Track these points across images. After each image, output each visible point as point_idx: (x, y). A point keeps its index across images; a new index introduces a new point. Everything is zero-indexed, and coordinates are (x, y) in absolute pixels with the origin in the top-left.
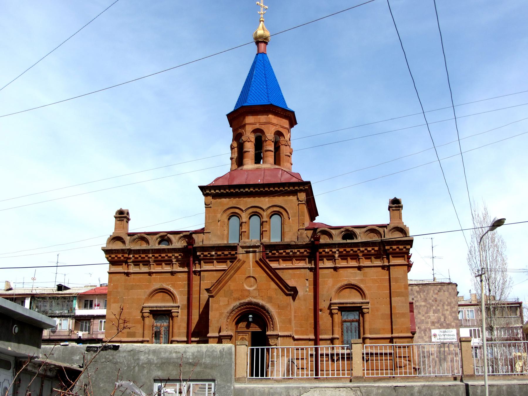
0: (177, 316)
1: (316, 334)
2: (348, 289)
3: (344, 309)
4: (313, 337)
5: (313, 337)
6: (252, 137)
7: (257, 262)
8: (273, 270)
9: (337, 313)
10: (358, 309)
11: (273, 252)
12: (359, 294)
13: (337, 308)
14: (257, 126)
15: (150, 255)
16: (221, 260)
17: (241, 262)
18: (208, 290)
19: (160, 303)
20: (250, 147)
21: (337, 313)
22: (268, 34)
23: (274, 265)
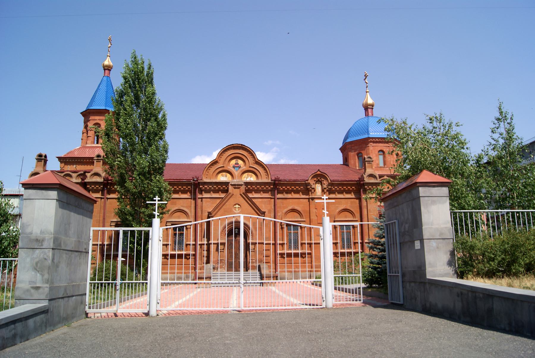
7: (241, 195)
8: (250, 199)
14: (96, 122)
16: (216, 191)
22: (111, 64)
23: (250, 195)
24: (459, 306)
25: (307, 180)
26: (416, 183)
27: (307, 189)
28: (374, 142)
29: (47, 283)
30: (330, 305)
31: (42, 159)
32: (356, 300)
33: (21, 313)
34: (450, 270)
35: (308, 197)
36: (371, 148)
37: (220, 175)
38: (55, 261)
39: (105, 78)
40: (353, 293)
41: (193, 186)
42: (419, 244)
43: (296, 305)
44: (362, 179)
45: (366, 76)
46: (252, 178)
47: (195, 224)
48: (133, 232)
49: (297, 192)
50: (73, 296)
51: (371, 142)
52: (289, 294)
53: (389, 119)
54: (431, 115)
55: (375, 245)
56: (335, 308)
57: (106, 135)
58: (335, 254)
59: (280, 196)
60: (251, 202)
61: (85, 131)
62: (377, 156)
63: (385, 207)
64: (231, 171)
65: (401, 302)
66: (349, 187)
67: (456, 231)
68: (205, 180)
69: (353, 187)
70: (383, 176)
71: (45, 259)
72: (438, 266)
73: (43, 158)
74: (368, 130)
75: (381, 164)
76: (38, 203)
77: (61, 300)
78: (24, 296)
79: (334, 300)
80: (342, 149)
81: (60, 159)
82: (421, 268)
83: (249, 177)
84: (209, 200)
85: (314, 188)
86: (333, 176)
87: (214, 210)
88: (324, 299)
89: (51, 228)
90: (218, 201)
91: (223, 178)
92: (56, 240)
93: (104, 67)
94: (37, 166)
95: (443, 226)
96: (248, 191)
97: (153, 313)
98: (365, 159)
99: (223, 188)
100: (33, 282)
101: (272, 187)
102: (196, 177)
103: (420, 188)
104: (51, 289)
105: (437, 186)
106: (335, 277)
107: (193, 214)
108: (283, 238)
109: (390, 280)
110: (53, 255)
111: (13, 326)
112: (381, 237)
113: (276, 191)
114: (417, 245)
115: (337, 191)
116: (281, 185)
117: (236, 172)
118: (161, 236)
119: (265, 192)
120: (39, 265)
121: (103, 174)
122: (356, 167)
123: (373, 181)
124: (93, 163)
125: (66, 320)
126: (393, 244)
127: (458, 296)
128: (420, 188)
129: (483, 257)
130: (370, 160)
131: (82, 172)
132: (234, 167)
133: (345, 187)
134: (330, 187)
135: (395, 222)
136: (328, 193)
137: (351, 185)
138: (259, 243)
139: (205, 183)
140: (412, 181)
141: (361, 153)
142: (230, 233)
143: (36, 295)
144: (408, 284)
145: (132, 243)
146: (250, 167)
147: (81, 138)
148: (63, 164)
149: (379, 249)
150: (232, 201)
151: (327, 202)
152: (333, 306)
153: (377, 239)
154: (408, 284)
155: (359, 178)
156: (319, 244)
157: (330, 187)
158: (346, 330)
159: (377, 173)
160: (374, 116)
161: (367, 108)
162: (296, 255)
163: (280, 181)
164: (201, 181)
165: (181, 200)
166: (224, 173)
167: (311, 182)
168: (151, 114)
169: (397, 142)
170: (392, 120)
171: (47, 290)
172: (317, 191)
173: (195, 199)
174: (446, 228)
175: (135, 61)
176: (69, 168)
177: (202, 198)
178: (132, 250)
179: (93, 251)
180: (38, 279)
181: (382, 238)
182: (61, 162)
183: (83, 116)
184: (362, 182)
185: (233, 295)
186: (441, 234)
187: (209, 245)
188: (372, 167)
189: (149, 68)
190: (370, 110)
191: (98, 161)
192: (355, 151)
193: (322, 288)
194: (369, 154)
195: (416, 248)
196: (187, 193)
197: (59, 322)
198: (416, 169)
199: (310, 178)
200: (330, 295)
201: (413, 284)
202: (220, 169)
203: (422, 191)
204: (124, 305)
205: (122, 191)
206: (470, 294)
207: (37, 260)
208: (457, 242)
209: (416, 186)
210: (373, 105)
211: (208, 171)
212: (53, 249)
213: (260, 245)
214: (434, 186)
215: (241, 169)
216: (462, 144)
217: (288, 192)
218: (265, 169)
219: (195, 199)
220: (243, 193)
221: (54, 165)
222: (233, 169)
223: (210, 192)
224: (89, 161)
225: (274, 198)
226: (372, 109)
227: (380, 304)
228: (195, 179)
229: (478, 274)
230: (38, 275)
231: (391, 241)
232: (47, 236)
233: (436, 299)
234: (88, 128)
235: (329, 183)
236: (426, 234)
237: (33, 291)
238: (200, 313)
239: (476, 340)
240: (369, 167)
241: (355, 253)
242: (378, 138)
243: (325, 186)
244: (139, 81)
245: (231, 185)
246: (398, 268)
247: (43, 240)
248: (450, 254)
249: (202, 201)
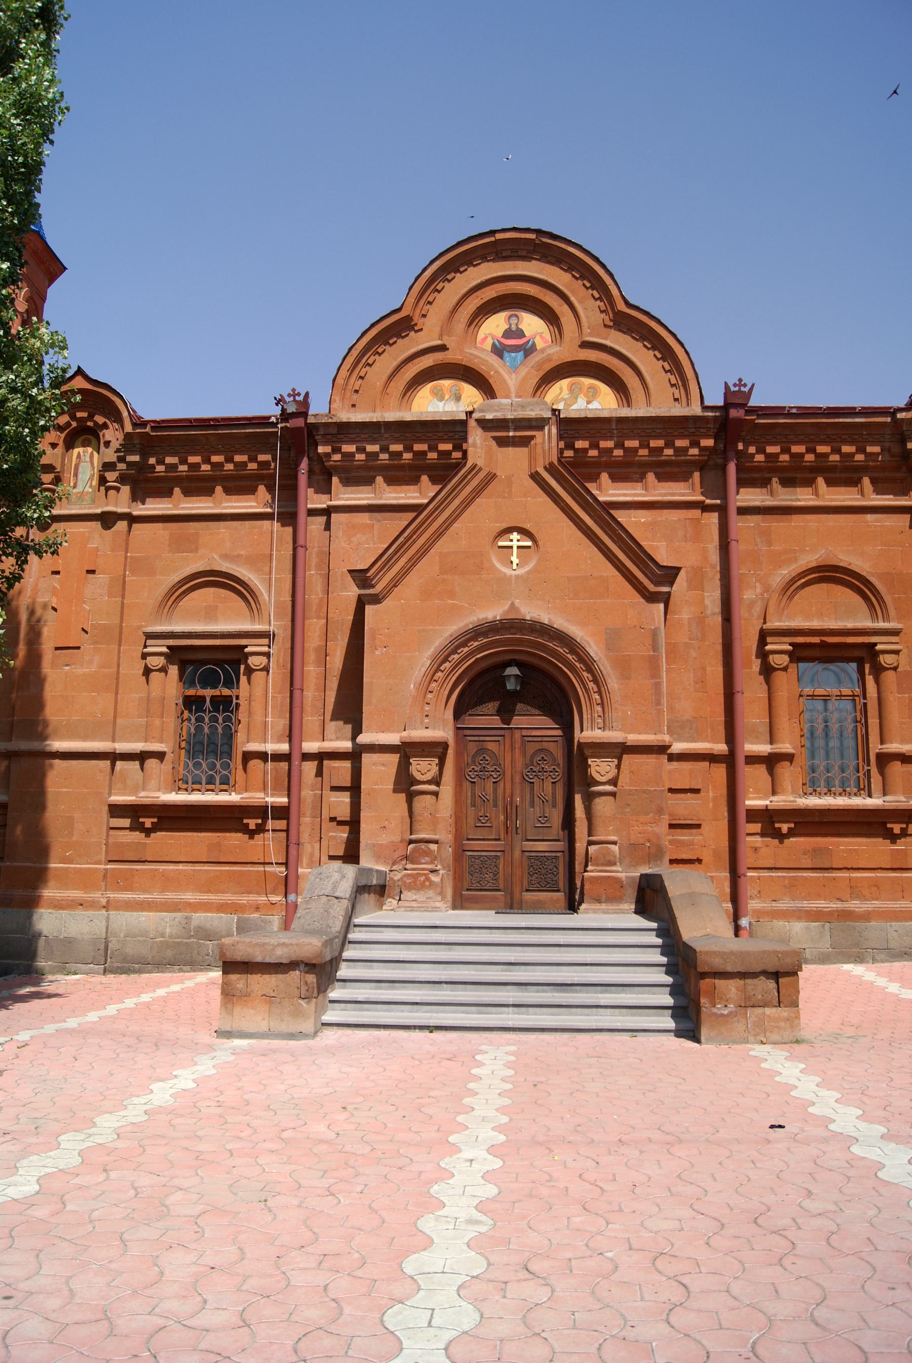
0: (266, 669)
1: (731, 737)
2: (824, 586)
3: (817, 650)
4: (721, 748)
5: (721, 748)
7: (535, 477)
8: (604, 512)
9: (785, 669)
10: (862, 655)
11: (653, 443)
12: (858, 599)
13: (165, 650)
16: (400, 475)
17: (481, 475)
18: (361, 577)
19: (212, 618)
21: (785, 669)
23: (608, 491)
37: (426, 390)
46: (598, 401)
50: (778, 993)
64: (482, 369)
91: (435, 403)
102: (294, 394)
113: (732, 468)
117: (512, 377)
119: (670, 471)
132: (499, 351)
139: (345, 431)
146: (585, 345)
150: (484, 514)
165: (222, 528)
166: (446, 383)
177: (327, 512)
196: (252, 491)
202: (427, 361)
215: (535, 359)
220: (550, 469)
222: (493, 360)
223: (369, 481)
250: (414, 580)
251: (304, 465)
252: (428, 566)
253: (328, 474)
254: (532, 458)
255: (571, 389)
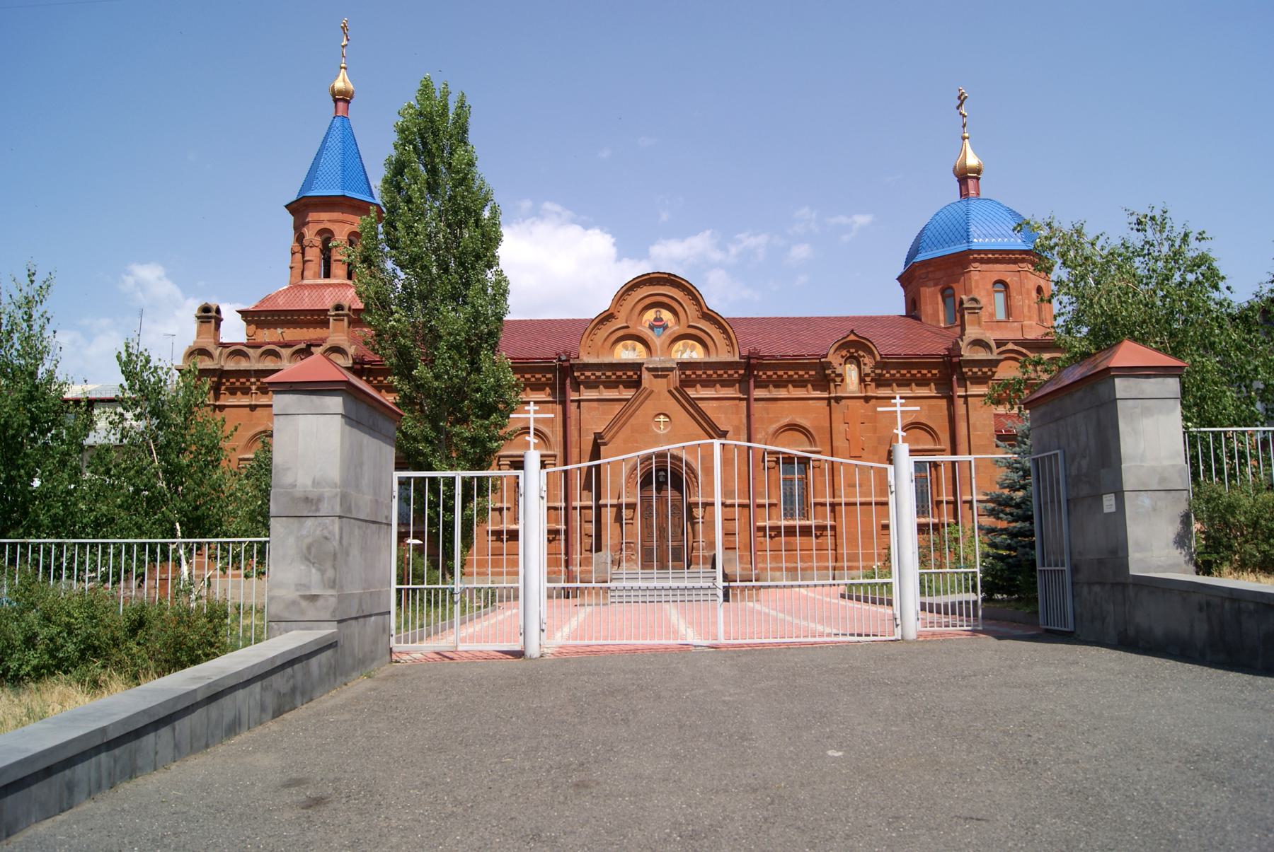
6: (318, 241)
7: (670, 392)
8: (692, 402)
14: (322, 226)
15: (253, 380)
18: (598, 436)
20: (314, 254)
22: (351, 87)
23: (692, 393)
24: (1201, 630)
25: (826, 356)
26: (1108, 369)
27: (824, 378)
28: (982, 261)
29: (333, 587)
30: (911, 635)
31: (209, 316)
32: (954, 626)
33: (301, 647)
34: (1179, 556)
35: (825, 395)
36: (975, 276)
38: (345, 543)
39: (338, 122)
40: (946, 613)
41: (560, 374)
42: (1113, 502)
43: (821, 635)
44: (954, 351)
45: (962, 99)
46: (694, 353)
47: (566, 464)
48: (433, 480)
49: (800, 383)
50: (370, 616)
51: (975, 260)
52: (801, 611)
53: (1040, 221)
54: (1142, 210)
55: (1000, 504)
56: (922, 640)
57: (363, 262)
58: (922, 529)
59: (759, 393)
60: (692, 407)
61: (298, 248)
62: (989, 295)
63: (1033, 420)
64: (645, 337)
65: (1070, 628)
66: (925, 372)
67: (1195, 475)
68: (587, 359)
69: (934, 372)
70: (1005, 344)
71: (326, 538)
72: (1155, 546)
73: (213, 314)
74: (967, 231)
75: (1001, 315)
76: (304, 422)
77: (353, 622)
78: (286, 615)
79: (919, 623)
80: (905, 280)
81: (245, 314)
82: (1118, 552)
83: (688, 351)
84: (595, 404)
85: (840, 375)
86: (886, 345)
87: (609, 428)
88: (899, 622)
89: (334, 472)
90: (618, 407)
91: (627, 353)
92: (344, 498)
93: (334, 95)
94: (198, 335)
95: (1166, 463)
96: (686, 383)
97: (533, 651)
98: (961, 302)
99: (630, 375)
100: (304, 585)
101: (742, 372)
102: (565, 352)
103: (1117, 380)
104: (341, 598)
105: (1155, 376)
106: (921, 574)
107: (559, 438)
108: (769, 490)
109: (1039, 578)
110: (341, 529)
111: (289, 670)
112: (1013, 488)
114: (1109, 503)
115: (895, 380)
116: (764, 366)
117: (657, 340)
118: (545, 488)
119: (726, 384)
120: (313, 550)
121: (351, 350)
122: (938, 321)
123: (982, 355)
124: (325, 324)
125: (362, 663)
126: (1052, 501)
127: (1201, 609)
128: (1117, 380)
129: (1255, 528)
130: (974, 305)
131: (303, 346)
132: (652, 327)
133: (914, 372)
134: (878, 371)
135: (1056, 455)
136: (873, 384)
137: (930, 366)
138: (861, 504)
140: (1095, 367)
141: (952, 288)
142: (646, 482)
143: (311, 612)
144: (1085, 590)
145: (434, 506)
146: (690, 326)
147: (289, 264)
148: (253, 327)
149: (1011, 514)
150: (649, 407)
151: (902, 412)
152: (919, 636)
153: (1006, 491)
154: (1085, 590)
155: (948, 349)
156: (886, 504)
157: (878, 371)
158: (964, 678)
159: (990, 336)
160: (982, 196)
161: (964, 177)
162: (806, 531)
163: (761, 358)
164: (577, 361)
167: (835, 359)
168: (467, 209)
169: (1035, 258)
170: (1049, 225)
171: (333, 601)
172: (848, 380)
173: (563, 403)
174: (1173, 466)
175: (426, 90)
176: (266, 335)
177: (579, 401)
178: (433, 523)
179: (725, 520)
180: (314, 580)
181: (1018, 490)
182: (248, 323)
183: (292, 212)
184: (955, 360)
185: (671, 618)
186: (1163, 480)
187: (599, 508)
188: (979, 324)
189: (462, 106)
190: (971, 183)
191: (338, 318)
192: (935, 285)
193: (881, 601)
194: (970, 291)
195: (1106, 510)
196: (543, 389)
197: (353, 669)
198: (1107, 335)
199: (832, 351)
200: (909, 614)
201: (1097, 588)
202: (621, 333)
203: (1122, 386)
204: (470, 629)
205: (406, 388)
206: (1227, 605)
207: (309, 540)
208: (1197, 495)
209: (1108, 374)
210: (978, 171)
211: (592, 337)
212: (340, 517)
213: (864, 507)
214: (1148, 376)
215: (668, 332)
216: (1213, 278)
217: (780, 384)
218: (725, 331)
219: (563, 403)
220: (676, 389)
221: (234, 330)
222: (649, 332)
224: (318, 318)
225: (748, 400)
226: (978, 179)
227: (1019, 632)
228: (563, 358)
229: (1243, 566)
230: (314, 570)
231: (1045, 495)
232: (328, 492)
233: (1149, 616)
234: (306, 242)
235: (877, 363)
236: (1129, 480)
237: (304, 604)
238: (633, 651)
239: (1242, 691)
240: (972, 324)
241: (936, 527)
242: (993, 252)
243: (867, 370)
244: (434, 140)
245: (648, 369)
246: (1062, 554)
247: (320, 499)
248: (1182, 522)
249: (579, 407)
250: (621, 435)
251: (568, 381)
252: (626, 430)
253: (578, 384)
254: (668, 384)
255: (684, 345)
